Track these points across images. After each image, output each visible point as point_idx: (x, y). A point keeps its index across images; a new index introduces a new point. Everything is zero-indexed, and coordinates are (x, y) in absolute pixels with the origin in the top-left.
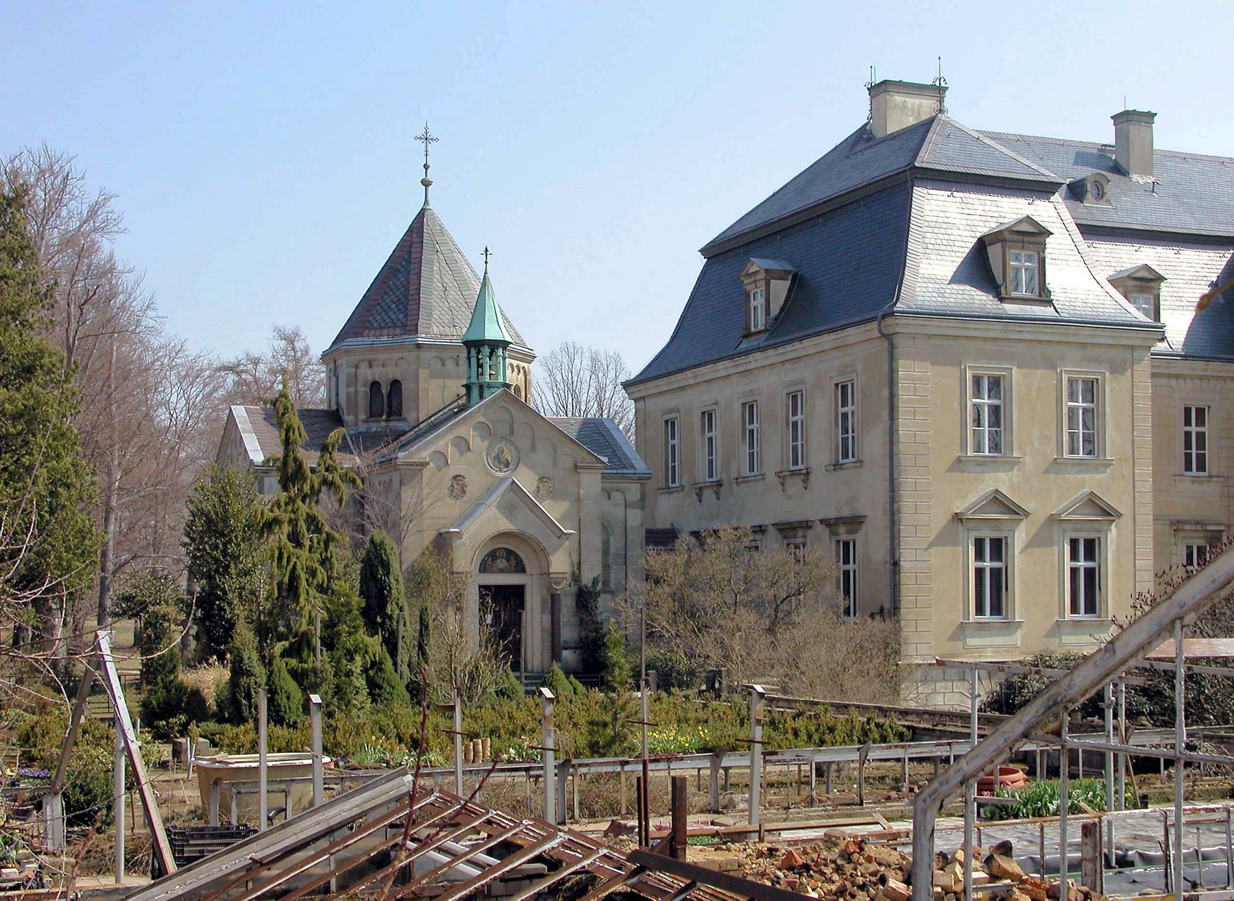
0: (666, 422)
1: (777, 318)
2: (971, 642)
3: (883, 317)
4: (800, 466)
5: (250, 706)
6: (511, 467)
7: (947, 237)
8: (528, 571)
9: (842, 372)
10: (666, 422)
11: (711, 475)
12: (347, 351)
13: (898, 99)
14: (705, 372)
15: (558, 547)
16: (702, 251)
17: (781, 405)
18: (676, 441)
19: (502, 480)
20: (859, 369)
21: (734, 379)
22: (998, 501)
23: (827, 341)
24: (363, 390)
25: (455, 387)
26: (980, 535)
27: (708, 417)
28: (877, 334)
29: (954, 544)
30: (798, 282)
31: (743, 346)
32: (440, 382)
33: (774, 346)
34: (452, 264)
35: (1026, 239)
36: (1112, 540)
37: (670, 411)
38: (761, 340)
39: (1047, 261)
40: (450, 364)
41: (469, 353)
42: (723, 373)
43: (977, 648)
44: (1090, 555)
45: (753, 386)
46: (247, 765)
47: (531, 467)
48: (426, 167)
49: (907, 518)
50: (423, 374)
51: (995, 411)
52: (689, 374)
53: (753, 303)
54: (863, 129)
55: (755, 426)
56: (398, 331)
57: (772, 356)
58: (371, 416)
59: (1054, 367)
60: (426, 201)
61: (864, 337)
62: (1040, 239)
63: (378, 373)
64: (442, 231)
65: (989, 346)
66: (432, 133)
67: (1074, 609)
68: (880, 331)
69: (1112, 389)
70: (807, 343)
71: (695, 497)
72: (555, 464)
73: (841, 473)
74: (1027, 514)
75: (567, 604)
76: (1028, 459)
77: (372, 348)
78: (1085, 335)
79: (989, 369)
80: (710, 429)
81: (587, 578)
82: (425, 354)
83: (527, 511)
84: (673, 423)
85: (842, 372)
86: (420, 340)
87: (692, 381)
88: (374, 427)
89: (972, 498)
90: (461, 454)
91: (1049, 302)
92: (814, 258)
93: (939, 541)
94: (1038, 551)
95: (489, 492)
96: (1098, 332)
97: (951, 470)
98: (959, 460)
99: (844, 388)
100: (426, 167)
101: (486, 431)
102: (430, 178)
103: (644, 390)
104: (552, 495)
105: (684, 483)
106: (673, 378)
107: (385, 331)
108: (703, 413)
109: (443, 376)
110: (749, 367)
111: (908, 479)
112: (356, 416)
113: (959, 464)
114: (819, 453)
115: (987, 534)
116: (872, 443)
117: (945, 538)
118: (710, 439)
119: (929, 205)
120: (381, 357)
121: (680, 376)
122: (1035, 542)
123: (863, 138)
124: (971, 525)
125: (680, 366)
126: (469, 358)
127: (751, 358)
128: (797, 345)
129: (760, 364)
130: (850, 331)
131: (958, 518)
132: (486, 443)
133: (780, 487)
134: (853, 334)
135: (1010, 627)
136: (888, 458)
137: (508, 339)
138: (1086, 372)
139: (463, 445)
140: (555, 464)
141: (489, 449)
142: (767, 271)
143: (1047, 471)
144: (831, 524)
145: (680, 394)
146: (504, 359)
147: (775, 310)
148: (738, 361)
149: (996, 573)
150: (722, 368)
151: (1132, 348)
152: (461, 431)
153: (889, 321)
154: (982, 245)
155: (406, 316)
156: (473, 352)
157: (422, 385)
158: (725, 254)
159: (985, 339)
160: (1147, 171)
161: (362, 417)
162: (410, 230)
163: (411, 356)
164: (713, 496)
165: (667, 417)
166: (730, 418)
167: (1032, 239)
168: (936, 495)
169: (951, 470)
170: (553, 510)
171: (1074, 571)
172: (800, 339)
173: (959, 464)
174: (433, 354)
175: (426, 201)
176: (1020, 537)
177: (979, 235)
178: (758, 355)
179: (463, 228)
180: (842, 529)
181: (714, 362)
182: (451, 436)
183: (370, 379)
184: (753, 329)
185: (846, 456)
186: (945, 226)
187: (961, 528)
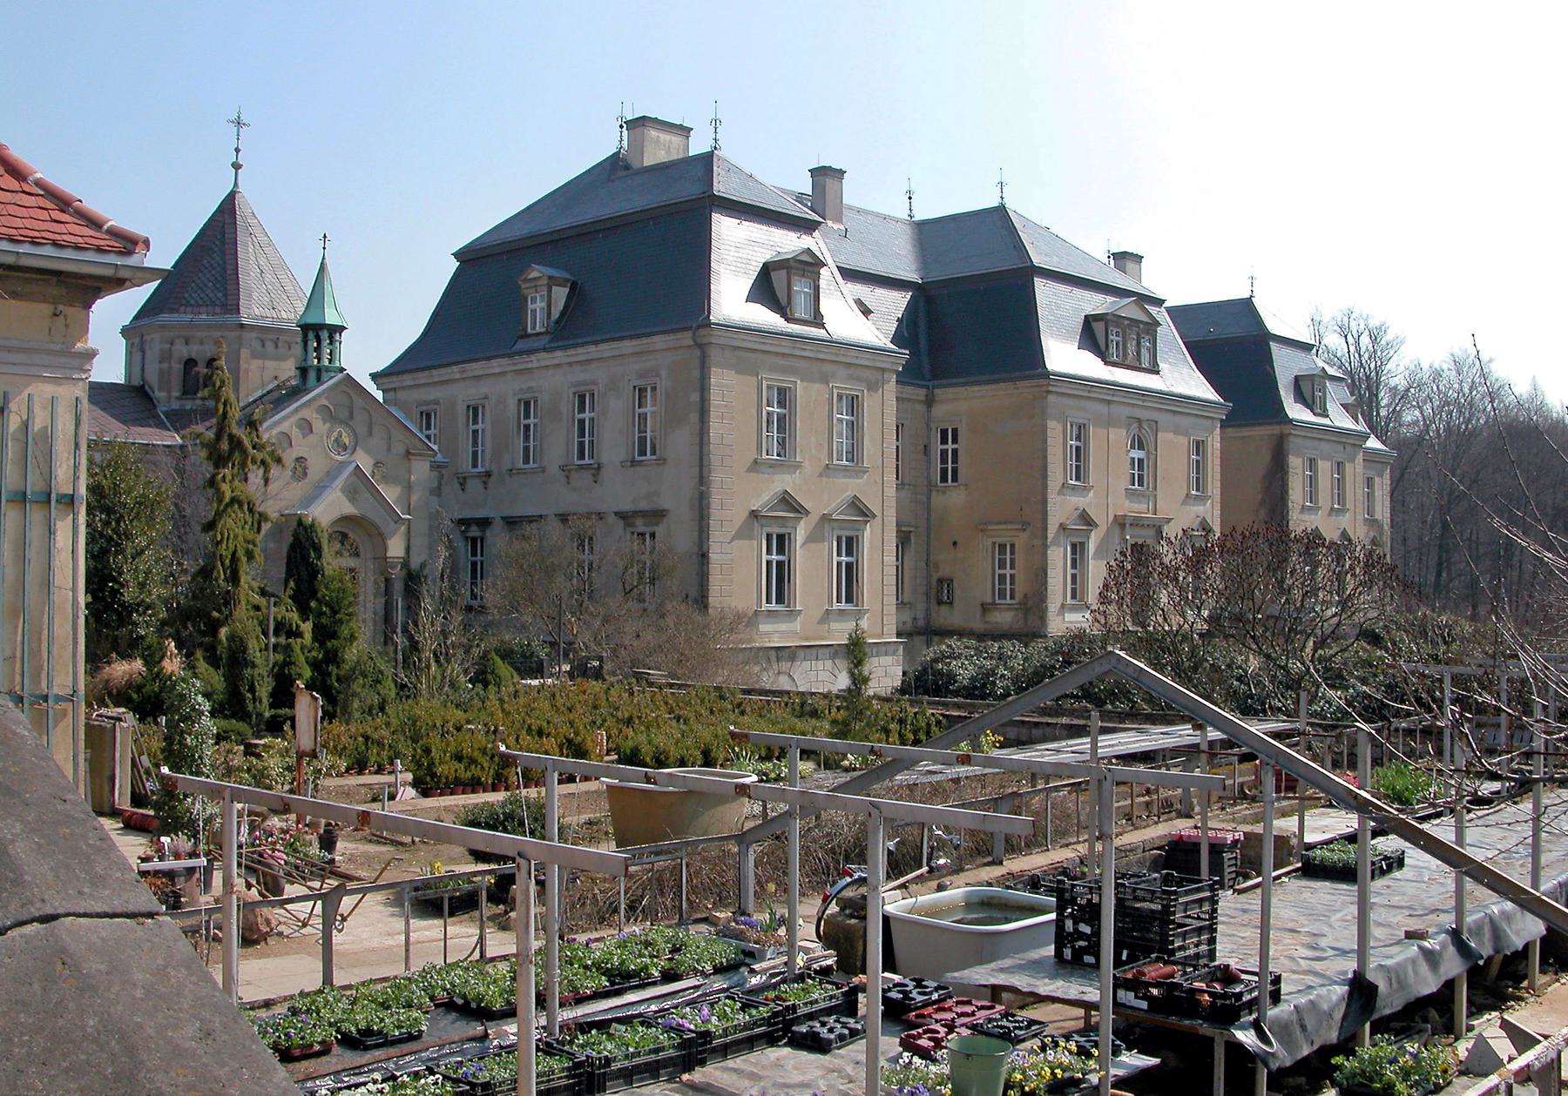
1: (558, 322)
2: (764, 628)
3: (699, 327)
4: (587, 461)
5: (254, 699)
9: (641, 376)
11: (475, 465)
12: (162, 327)
13: (653, 133)
15: (395, 532)
16: (457, 255)
17: (567, 405)
19: (343, 465)
20: (664, 374)
21: (509, 377)
22: (787, 501)
24: (178, 367)
25: (287, 370)
26: (770, 530)
27: (474, 411)
29: (751, 538)
30: (574, 287)
32: (259, 362)
36: (868, 535)
37: (428, 403)
40: (270, 346)
42: (497, 370)
43: (767, 633)
44: (781, 551)
45: (533, 384)
46: (118, 755)
47: (368, 452)
48: (237, 150)
49: (715, 514)
50: (245, 353)
51: (782, 418)
52: (455, 369)
54: (616, 155)
56: (218, 310)
58: (184, 393)
59: (827, 383)
60: (236, 184)
61: (671, 345)
63: (194, 350)
65: (782, 362)
66: (244, 119)
67: (839, 601)
69: (870, 403)
72: (389, 449)
73: (638, 469)
74: (807, 513)
75: (398, 587)
76: (806, 463)
77: (191, 325)
79: (785, 380)
81: (415, 563)
82: (247, 335)
85: (641, 376)
86: (245, 321)
88: (189, 405)
89: (765, 497)
90: (304, 436)
91: (822, 326)
93: (739, 535)
94: (813, 546)
95: (331, 476)
97: (749, 470)
98: (756, 462)
100: (237, 150)
101: (329, 415)
103: (394, 381)
104: (385, 479)
106: (435, 372)
107: (203, 309)
109: (263, 356)
111: (717, 476)
112: (169, 393)
113: (756, 465)
114: (613, 446)
115: (776, 530)
116: (680, 443)
117: (744, 533)
119: (725, 228)
121: (443, 371)
122: (812, 538)
123: (615, 165)
124: (764, 521)
127: (533, 357)
129: (543, 363)
130: (656, 338)
131: (754, 515)
132: (328, 425)
134: (659, 341)
135: (792, 614)
138: (851, 388)
139: (306, 427)
140: (389, 449)
141: (330, 431)
142: (550, 278)
143: (820, 475)
144: (625, 517)
147: (555, 314)
149: (780, 564)
151: (883, 370)
152: (305, 414)
153: (702, 332)
154: (767, 271)
157: (243, 366)
158: (469, 258)
159: (777, 354)
160: (839, 220)
161: (176, 394)
163: (232, 335)
164: (480, 486)
168: (738, 494)
169: (749, 470)
170: (390, 494)
171: (769, 563)
172: (596, 343)
173: (756, 465)
174: (254, 335)
175: (236, 184)
176: (801, 533)
178: (543, 355)
180: (639, 522)
182: (294, 419)
183: (186, 356)
185: (643, 452)
186: (737, 252)
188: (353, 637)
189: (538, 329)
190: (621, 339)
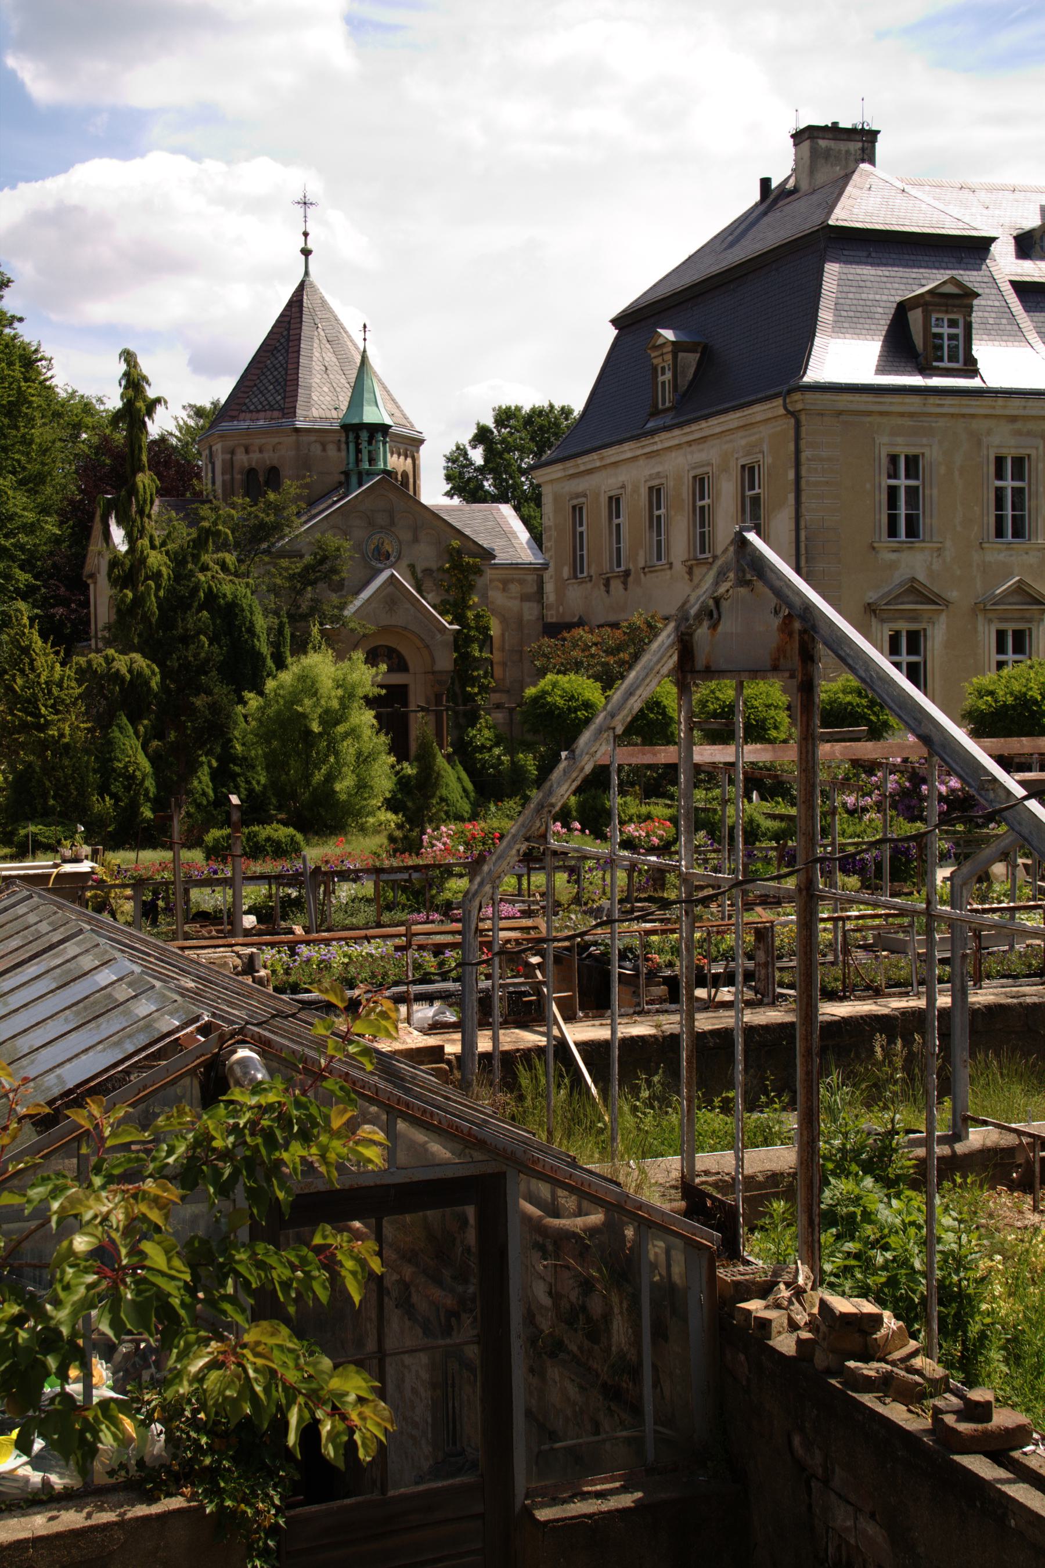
0: (574, 507)
1: (684, 395)
3: (789, 392)
6: (392, 559)
7: (862, 303)
8: (411, 669)
10: (574, 507)
14: (612, 454)
16: (615, 322)
17: (686, 492)
18: (584, 528)
20: (765, 448)
22: (914, 591)
23: (733, 419)
27: (614, 502)
28: (782, 411)
30: (707, 355)
31: (649, 425)
33: (680, 425)
34: (336, 338)
35: (950, 302)
37: (578, 496)
38: (668, 420)
39: (974, 326)
41: (347, 437)
42: (629, 455)
48: (306, 234)
52: (594, 456)
53: (661, 379)
55: (662, 511)
57: (675, 437)
60: (307, 273)
62: (966, 301)
64: (324, 303)
66: (299, 197)
68: (786, 409)
70: (713, 421)
71: (602, 588)
74: (947, 603)
78: (1015, 407)
80: (618, 516)
83: (408, 606)
84: (581, 509)
86: (299, 425)
87: (598, 464)
92: (714, 333)
96: (1030, 403)
99: (752, 470)
100: (306, 234)
102: (310, 246)
105: (592, 573)
106: (579, 461)
107: (262, 414)
108: (610, 498)
110: (655, 448)
115: (903, 626)
118: (618, 526)
120: (258, 441)
121: (586, 459)
125: (588, 447)
126: (347, 443)
128: (703, 424)
129: (667, 444)
130: (757, 408)
133: (687, 577)
136: (793, 545)
137: (388, 421)
145: (587, 477)
146: (384, 443)
148: (645, 441)
150: (627, 450)
154: (902, 309)
155: (284, 398)
156: (351, 437)
158: (634, 322)
159: (902, 415)
162: (290, 304)
164: (621, 586)
165: (575, 502)
166: (635, 504)
167: (957, 302)
175: (307, 273)
177: (898, 299)
178: (664, 435)
179: (345, 306)
181: (620, 442)
184: (660, 406)
187: (873, 619)
188: (981, 693)
189: (667, 404)
190: (726, 411)
